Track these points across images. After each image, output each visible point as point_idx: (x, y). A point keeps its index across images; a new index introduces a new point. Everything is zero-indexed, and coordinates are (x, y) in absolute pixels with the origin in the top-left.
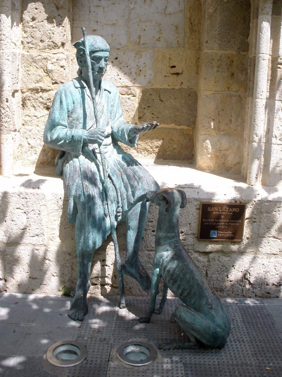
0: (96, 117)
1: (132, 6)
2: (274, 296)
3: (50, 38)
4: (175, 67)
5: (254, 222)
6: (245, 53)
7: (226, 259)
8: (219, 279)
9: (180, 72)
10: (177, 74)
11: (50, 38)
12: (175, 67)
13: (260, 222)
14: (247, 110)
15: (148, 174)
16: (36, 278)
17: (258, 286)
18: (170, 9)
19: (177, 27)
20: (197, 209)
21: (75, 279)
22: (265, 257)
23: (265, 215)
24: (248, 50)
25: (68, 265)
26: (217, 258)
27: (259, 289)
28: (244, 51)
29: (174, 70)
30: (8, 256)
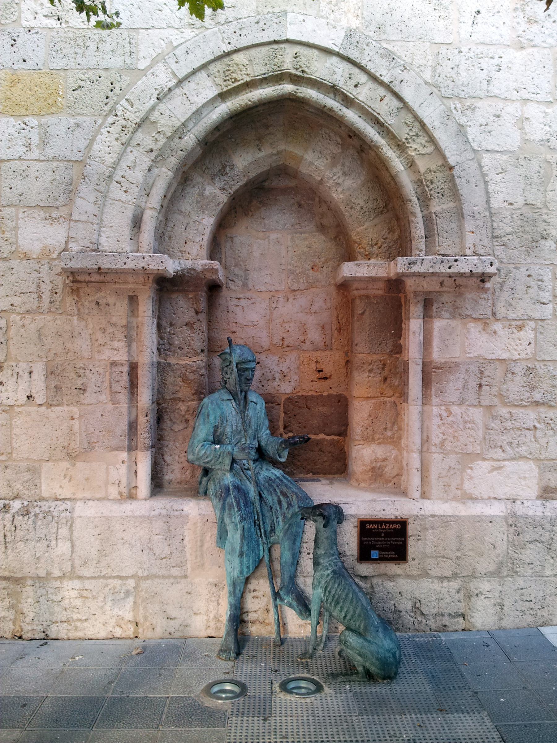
0: (31, 640)
1: (274, 306)
2: (451, 629)
3: (190, 345)
4: (322, 371)
5: (418, 540)
6: (398, 356)
7: (391, 584)
8: (385, 609)
9: (328, 376)
10: (325, 378)
11: (190, 345)
12: (322, 371)
13: (426, 539)
14: (403, 417)
15: (113, 72)
16: (175, 618)
17: (431, 617)
18: (315, 307)
19: (323, 327)
20: (354, 527)
21: (221, 616)
22: (436, 581)
23: (430, 531)
24: (401, 352)
25: (213, 599)
26: (380, 582)
27: (433, 620)
28: (397, 353)
29: (321, 375)
30: (143, 593)
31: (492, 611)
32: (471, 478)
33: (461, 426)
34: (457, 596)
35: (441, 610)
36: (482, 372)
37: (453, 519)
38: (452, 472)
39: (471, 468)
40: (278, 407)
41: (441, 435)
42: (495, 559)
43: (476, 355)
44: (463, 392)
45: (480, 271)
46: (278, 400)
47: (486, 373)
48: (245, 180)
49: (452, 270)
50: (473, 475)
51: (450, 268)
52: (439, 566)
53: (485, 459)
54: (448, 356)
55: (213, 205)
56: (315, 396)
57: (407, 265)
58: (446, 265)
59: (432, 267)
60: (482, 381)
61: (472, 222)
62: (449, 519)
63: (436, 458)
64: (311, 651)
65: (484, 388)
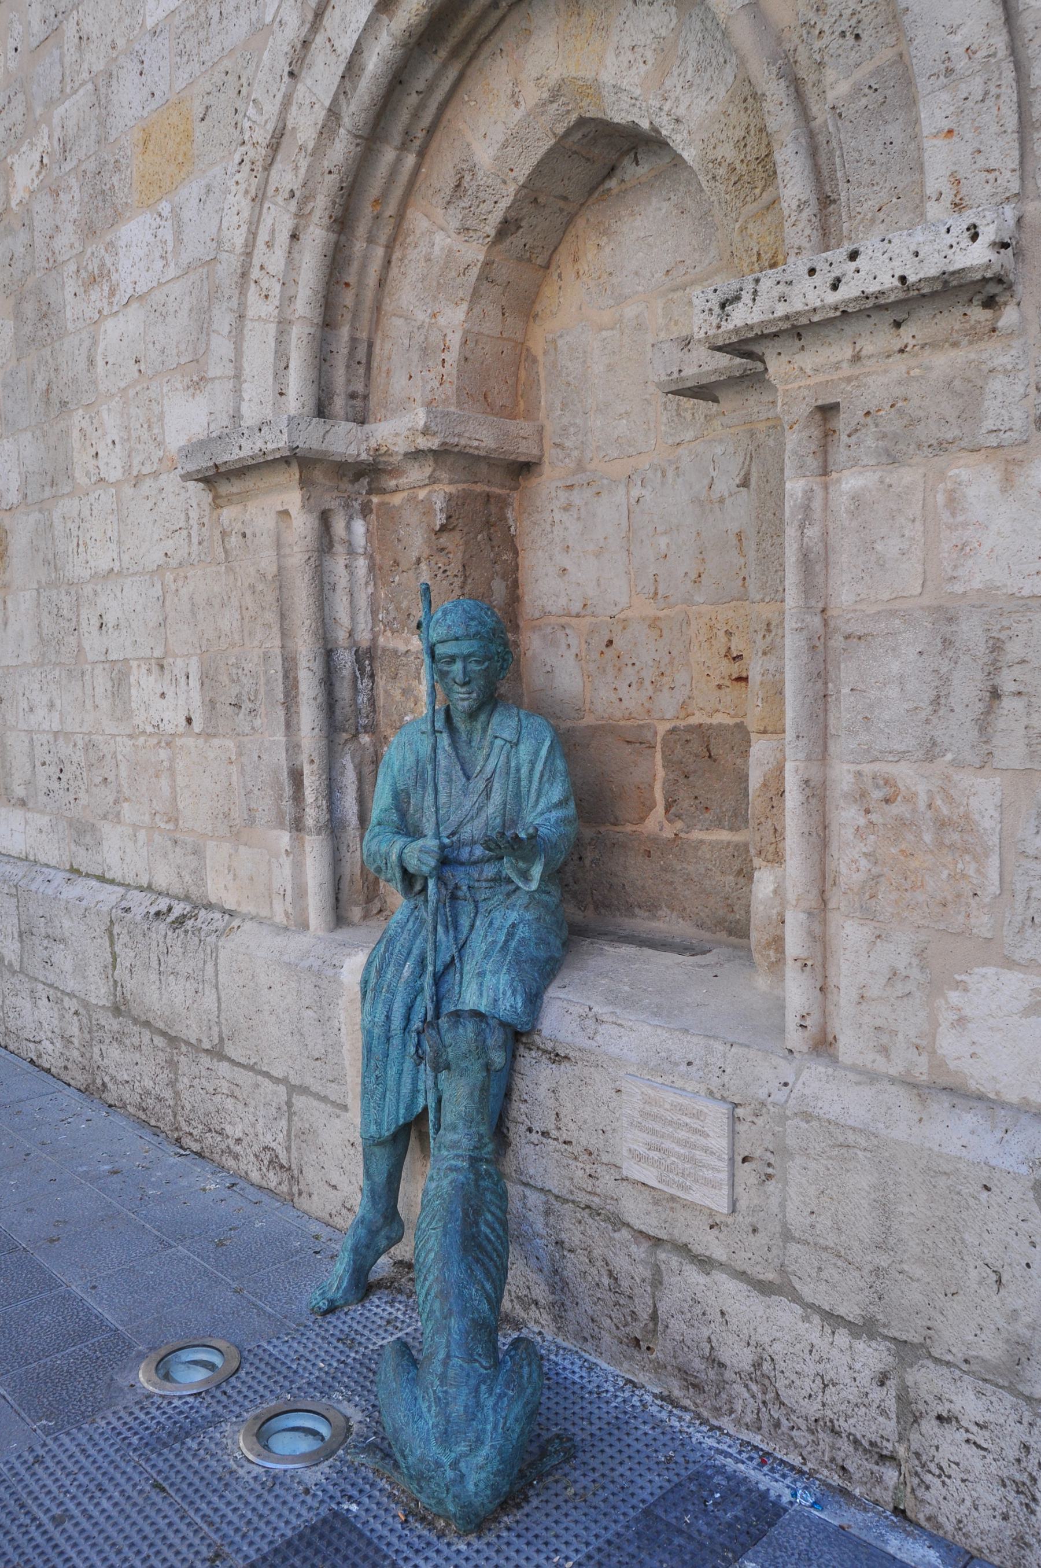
31: (993, 1500)
32: (961, 1021)
33: (928, 838)
34: (877, 1394)
35: (829, 1413)
36: (996, 647)
37: (862, 1142)
38: (900, 988)
39: (959, 985)
40: (648, 751)
41: (863, 863)
42: (1001, 1323)
43: (976, 584)
44: (935, 720)
45: (933, 271)
46: (649, 736)
47: (1014, 650)
48: (512, 189)
49: (846, 292)
50: (967, 1012)
51: (835, 287)
52: (824, 1275)
53: (1009, 963)
54: (886, 596)
55: (454, 274)
56: (727, 727)
57: (717, 310)
58: (822, 279)
59: (782, 298)
60: (997, 681)
61: (945, 96)
62: (851, 1137)
63: (850, 933)
64: (1020, 1387)
65: (1008, 703)
